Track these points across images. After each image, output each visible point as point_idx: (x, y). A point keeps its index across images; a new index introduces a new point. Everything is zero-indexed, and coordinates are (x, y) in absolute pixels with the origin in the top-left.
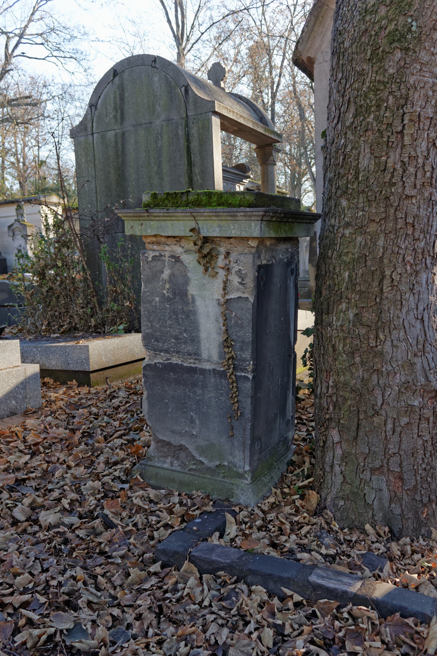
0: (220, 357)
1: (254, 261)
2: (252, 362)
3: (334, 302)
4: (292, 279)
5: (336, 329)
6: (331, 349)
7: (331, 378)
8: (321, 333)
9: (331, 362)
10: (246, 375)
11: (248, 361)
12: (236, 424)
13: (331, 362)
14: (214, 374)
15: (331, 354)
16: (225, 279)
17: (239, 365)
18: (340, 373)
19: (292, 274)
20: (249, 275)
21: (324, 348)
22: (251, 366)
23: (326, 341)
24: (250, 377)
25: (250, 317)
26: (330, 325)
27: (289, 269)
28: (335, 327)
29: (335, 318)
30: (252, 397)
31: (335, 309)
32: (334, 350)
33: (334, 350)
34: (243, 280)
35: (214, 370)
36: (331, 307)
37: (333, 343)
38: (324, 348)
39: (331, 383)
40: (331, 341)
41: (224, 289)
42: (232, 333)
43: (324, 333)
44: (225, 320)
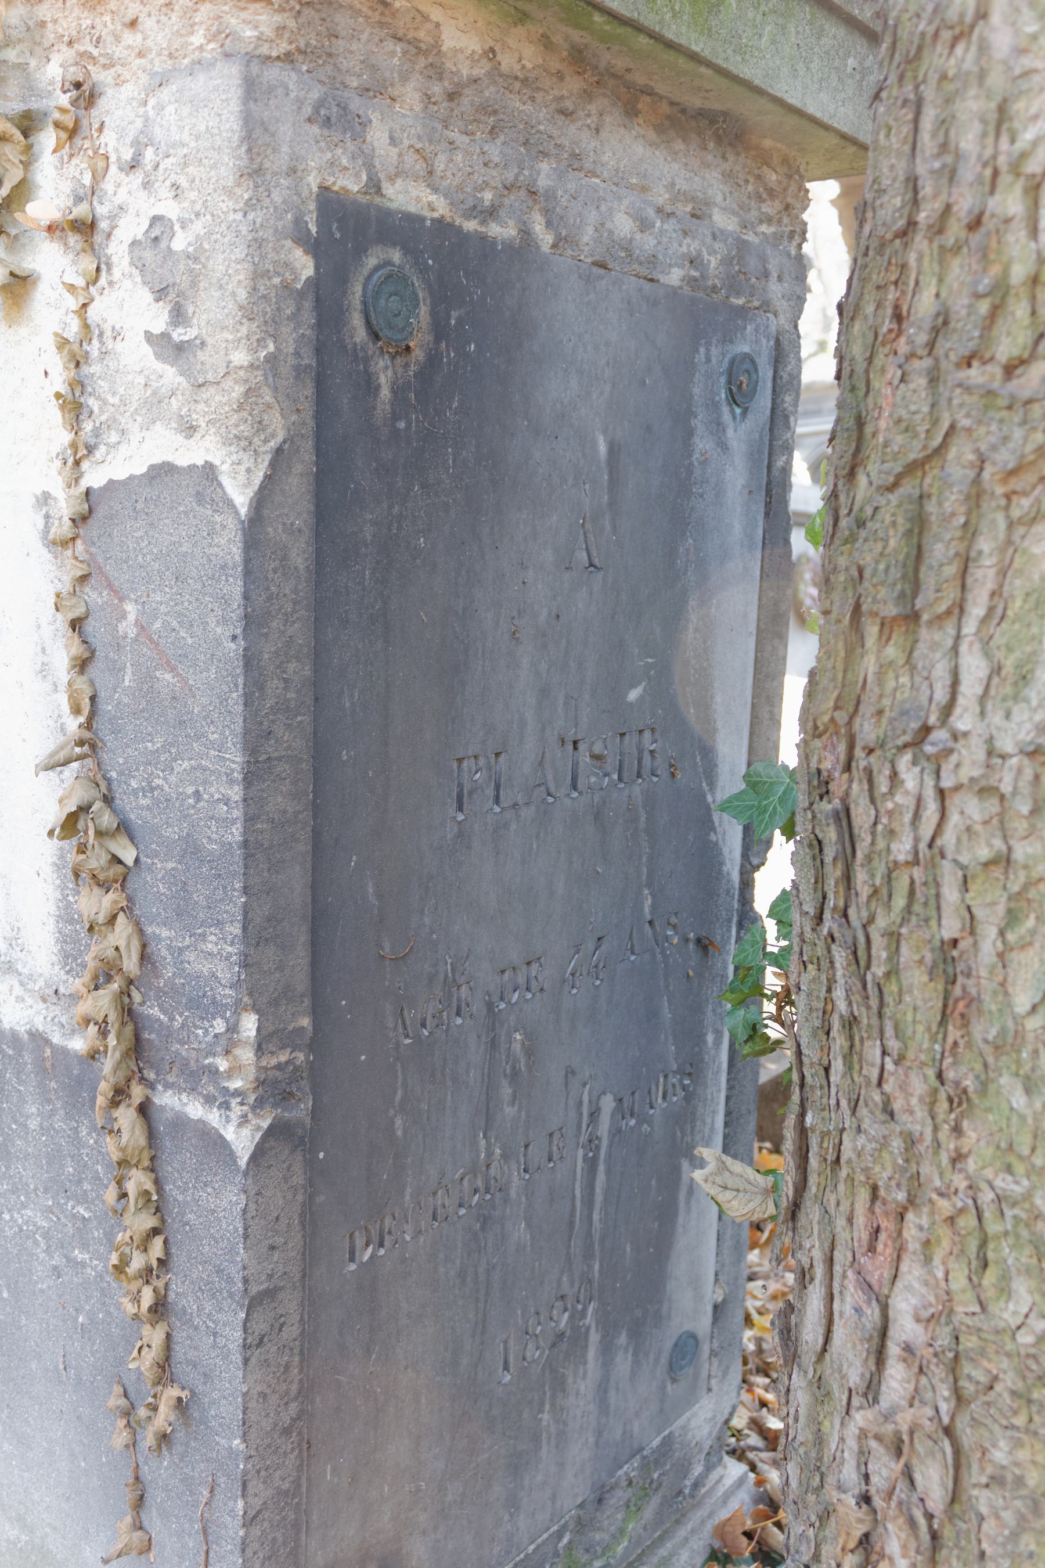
0: (69, 958)
1: (255, 135)
2: (250, 1025)
3: (976, 495)
4: (740, 434)
5: (985, 791)
6: (918, 992)
7: (911, 1271)
8: (844, 817)
9: (917, 1121)
10: (213, 1117)
11: (216, 1008)
12: (160, 1471)
13: (917, 1121)
14: (42, 1070)
15: (921, 1038)
16: (73, 329)
17: (168, 1034)
18: (1003, 1252)
19: (739, 396)
20: (218, 264)
21: (860, 961)
22: (246, 1055)
23: (882, 894)
24: (241, 1139)
25: (221, 635)
26: (150, 869)
27: (713, 358)
28: (969, 761)
29: (974, 668)
30: (254, 1304)
31: (984, 577)
32: (954, 1010)
33: (954, 1010)
34: (178, 316)
35: (38, 1038)
36: (940, 550)
37: (950, 927)
38: (860, 961)
39: (906, 1328)
40: (923, 902)
41: (73, 406)
42: (126, 773)
43: (862, 815)
44: (82, 665)
